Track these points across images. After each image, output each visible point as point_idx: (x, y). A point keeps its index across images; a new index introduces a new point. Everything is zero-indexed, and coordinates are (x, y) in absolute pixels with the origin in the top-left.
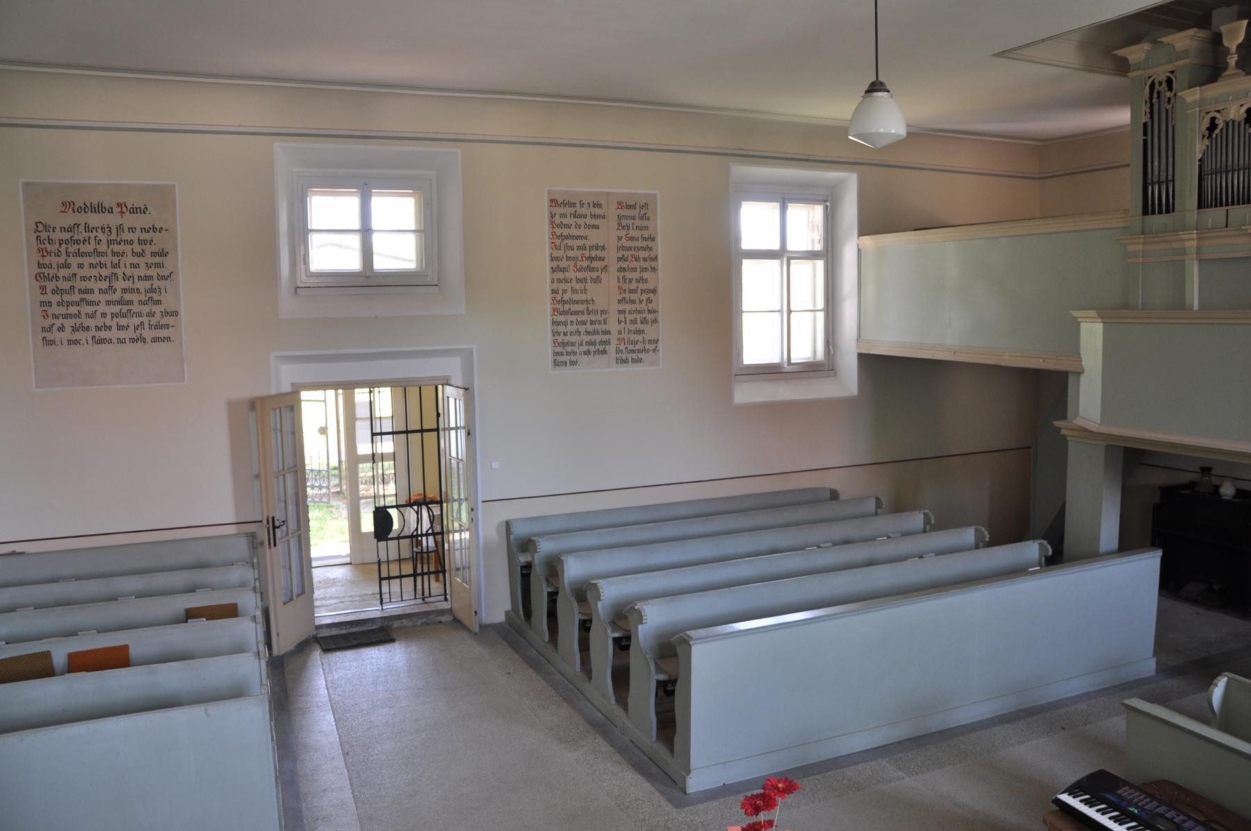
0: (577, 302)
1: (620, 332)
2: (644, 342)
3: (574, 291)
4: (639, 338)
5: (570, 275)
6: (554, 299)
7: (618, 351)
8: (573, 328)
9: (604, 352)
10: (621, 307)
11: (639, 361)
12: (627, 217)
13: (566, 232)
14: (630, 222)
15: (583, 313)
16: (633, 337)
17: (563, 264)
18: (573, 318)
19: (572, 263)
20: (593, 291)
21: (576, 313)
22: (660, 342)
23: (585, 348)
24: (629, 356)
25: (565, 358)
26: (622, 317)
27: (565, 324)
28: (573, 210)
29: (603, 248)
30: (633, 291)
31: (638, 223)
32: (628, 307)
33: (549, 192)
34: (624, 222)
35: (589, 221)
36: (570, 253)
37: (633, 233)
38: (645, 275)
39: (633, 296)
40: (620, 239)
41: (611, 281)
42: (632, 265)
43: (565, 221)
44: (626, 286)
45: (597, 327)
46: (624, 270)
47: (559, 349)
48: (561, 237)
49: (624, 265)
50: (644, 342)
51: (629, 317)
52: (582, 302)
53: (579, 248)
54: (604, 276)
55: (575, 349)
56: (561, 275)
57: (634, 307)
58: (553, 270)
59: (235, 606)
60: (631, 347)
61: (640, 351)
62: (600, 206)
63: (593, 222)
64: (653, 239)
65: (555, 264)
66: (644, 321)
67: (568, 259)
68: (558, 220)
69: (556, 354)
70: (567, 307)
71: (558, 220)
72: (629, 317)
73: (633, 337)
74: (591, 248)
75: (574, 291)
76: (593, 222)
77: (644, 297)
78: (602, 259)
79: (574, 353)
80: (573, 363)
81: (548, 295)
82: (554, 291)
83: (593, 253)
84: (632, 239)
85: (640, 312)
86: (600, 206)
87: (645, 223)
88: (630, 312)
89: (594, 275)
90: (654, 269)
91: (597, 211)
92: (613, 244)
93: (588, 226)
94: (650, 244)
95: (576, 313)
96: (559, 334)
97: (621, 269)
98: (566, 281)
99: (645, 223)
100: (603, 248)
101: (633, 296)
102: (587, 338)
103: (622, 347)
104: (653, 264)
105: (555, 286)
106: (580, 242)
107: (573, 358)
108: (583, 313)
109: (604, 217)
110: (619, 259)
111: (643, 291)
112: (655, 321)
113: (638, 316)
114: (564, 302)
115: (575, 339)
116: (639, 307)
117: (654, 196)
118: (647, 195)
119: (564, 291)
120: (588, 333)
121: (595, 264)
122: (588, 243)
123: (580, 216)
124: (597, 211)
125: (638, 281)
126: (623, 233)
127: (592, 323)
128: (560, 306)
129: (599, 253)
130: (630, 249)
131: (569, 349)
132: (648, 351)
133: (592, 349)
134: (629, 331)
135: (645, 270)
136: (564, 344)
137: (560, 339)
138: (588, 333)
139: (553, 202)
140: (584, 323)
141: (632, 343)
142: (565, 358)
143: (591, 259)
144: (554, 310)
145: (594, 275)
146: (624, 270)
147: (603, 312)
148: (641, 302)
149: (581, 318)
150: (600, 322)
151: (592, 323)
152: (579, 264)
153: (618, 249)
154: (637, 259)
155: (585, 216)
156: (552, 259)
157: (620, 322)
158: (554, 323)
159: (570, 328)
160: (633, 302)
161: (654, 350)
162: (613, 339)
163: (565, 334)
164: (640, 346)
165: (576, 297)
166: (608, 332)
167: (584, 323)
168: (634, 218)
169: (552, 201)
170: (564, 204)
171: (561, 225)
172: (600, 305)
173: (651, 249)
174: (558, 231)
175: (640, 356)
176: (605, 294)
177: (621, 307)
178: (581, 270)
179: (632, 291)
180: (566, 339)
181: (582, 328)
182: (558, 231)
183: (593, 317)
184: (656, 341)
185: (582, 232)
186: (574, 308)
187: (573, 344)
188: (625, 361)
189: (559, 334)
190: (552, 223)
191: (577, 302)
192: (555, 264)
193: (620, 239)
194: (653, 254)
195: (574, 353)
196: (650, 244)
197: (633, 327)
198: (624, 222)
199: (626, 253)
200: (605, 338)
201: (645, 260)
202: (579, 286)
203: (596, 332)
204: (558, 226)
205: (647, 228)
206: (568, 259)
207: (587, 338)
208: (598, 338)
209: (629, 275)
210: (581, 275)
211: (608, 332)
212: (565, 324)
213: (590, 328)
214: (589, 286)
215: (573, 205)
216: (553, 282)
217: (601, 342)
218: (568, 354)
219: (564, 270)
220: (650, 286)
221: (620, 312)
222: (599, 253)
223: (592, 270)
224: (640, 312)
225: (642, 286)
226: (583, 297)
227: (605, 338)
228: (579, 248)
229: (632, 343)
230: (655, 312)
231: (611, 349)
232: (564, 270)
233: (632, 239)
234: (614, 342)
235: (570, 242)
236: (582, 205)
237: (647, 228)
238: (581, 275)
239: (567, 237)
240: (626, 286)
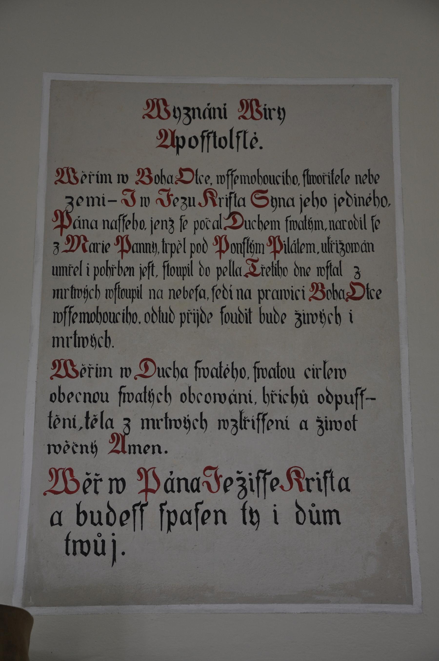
169: (60, 172)
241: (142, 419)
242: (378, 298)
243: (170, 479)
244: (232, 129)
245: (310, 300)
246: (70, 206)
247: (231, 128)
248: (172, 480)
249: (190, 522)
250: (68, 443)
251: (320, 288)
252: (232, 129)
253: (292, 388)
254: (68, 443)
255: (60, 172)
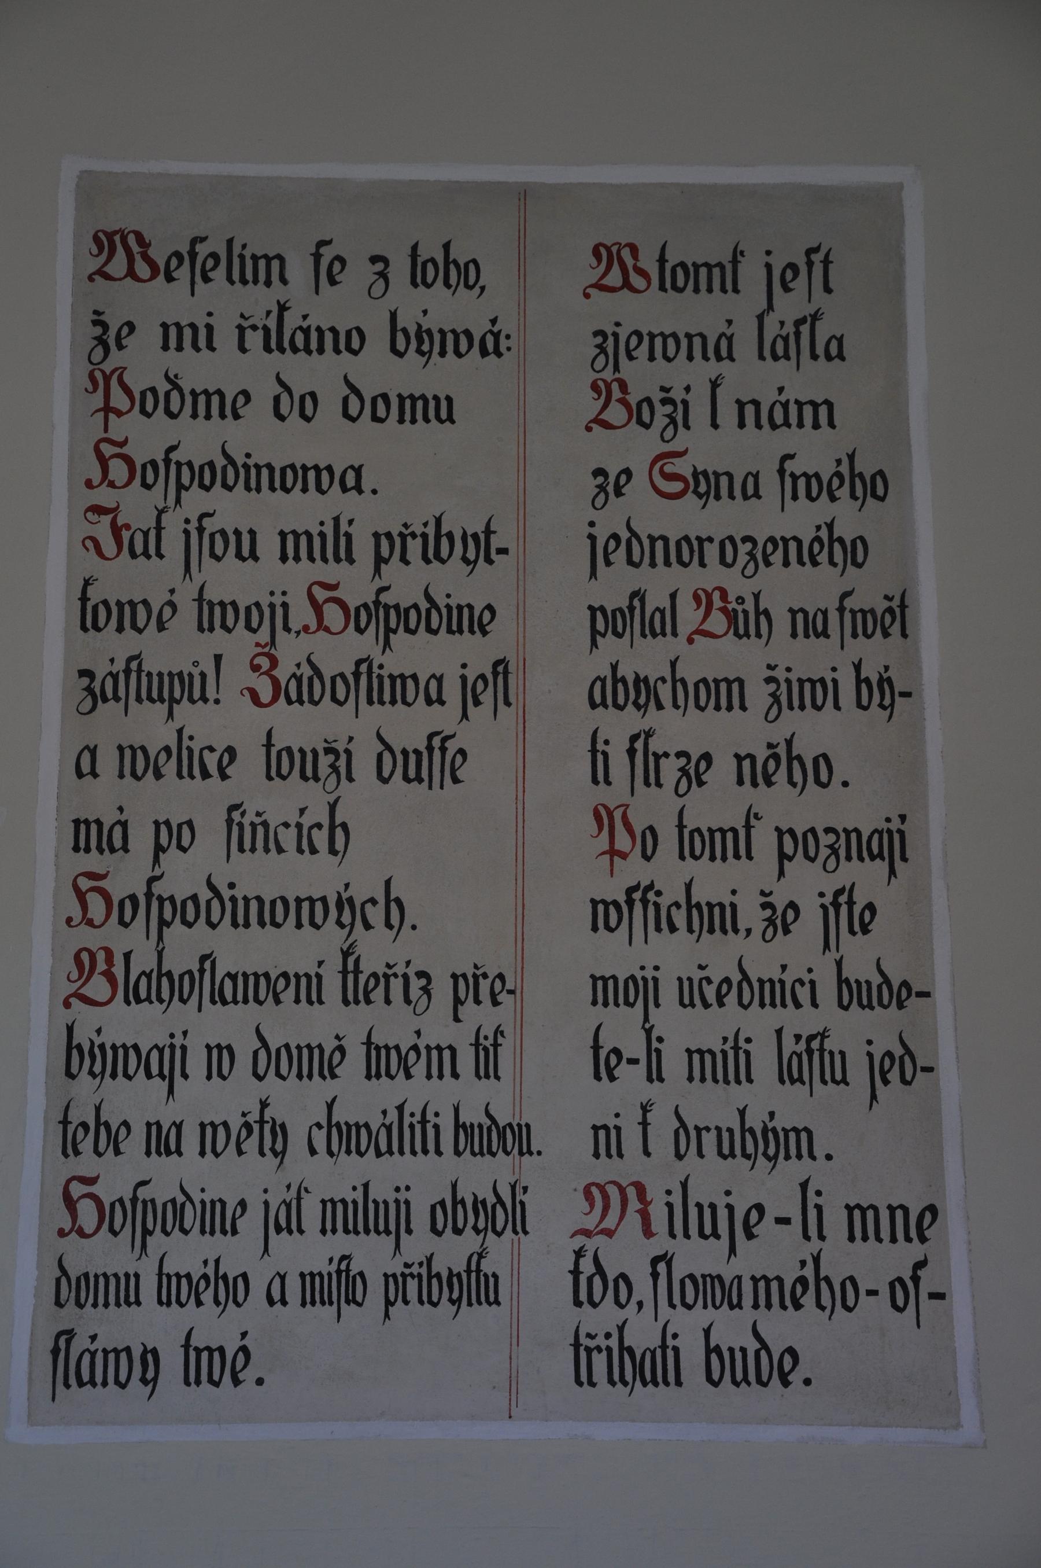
0: (268, 913)
1: (606, 1139)
2: (811, 1221)
3: (246, 833)
4: (775, 1186)
5: (226, 721)
6: (85, 888)
7: (592, 1282)
8: (232, 1099)
9: (475, 1286)
10: (618, 955)
11: (781, 1368)
12: (662, 345)
13: (199, 440)
14: (690, 375)
15: (309, 988)
16: (711, 1178)
17: (169, 651)
18: (232, 1024)
19: (238, 646)
20: (388, 831)
21: (256, 987)
22: (954, 1229)
23: (311, 1251)
24: (688, 1326)
25: (154, 1325)
26: (623, 1029)
27: (167, 1064)
28: (258, 301)
29: (482, 547)
30: (728, 843)
31: (751, 377)
32: (673, 955)
33: (90, 188)
34: (643, 377)
35: (379, 370)
36: (229, 580)
37: (705, 448)
38: (813, 731)
39: (713, 882)
40: (610, 484)
41: (535, 763)
42: (702, 661)
43: (197, 370)
44: (654, 808)
45: (417, 1091)
46: (643, 692)
47: (107, 1254)
48: (169, 470)
49: (645, 658)
50: (811, 1221)
51: (682, 1029)
52: (306, 911)
53: (294, 545)
54: (482, 734)
55: (238, 1253)
56: (151, 726)
57: (720, 956)
58: (94, 690)
59: (745, 426)
60: (698, 1257)
61: (771, 1292)
62: (460, 273)
63: (408, 375)
64: (873, 487)
65: (111, 647)
66: (809, 1062)
67: (213, 615)
68: (144, 363)
69: (73, 1288)
70: (183, 946)
71: (144, 363)
72: (682, 1029)
73: (711, 1178)
74: (390, 546)
75: (246, 833)
76: (408, 375)
77: (807, 884)
78: (474, 621)
79: (230, 1288)
80: (213, 1366)
81: (47, 859)
82: (88, 834)
83: (406, 583)
84: (707, 485)
85: (775, 993)
86: (460, 273)
87: (805, 381)
88: (691, 993)
89: (409, 726)
90: (882, 692)
91: (444, 308)
92: (563, 513)
93: (361, 405)
94: (849, 518)
95: (256, 987)
96: (110, 1137)
97: (612, 691)
98: (190, 761)
99: (805, 381)
100: (482, 547)
101: (713, 882)
102: (337, 1177)
103: (628, 1253)
104: (875, 654)
105: (102, 797)
106: (306, 511)
107: (214, 1325)
108: (309, 988)
109: (492, 345)
110: (605, 623)
111: (795, 844)
112: (900, 1066)
113: (759, 1024)
114: (164, 911)
115: (241, 1177)
116: (764, 959)
117: (886, 202)
118: (822, 196)
119: (174, 836)
120: (345, 1137)
121: (413, 654)
122: (366, 516)
123: (313, 341)
124: (444, 308)
125: (752, 771)
126: (635, 448)
127: (381, 1061)
128: (135, 941)
129: (453, 582)
130: (689, 550)
131: (187, 1253)
132: (846, 1294)
133: (373, 1256)
134: (687, 1136)
135: (815, 693)
136: (142, 1216)
137: (116, 1176)
138: (345, 1137)
139: (117, 250)
140: (319, 1062)
141: (704, 1221)
142: (154, 1325)
143: (384, 617)
144: (84, 964)
145: (409, 726)
146: (643, 692)
147: (471, 986)
148: (780, 920)
149: (290, 1024)
150: (442, 1061)
151: (381, 1061)
152: (291, 652)
153: (598, 556)
154: (746, 621)
155: (351, 341)
156: (90, 615)
157: (605, 1064)
158: (76, 1055)
159: (200, 1099)
160: (719, 919)
161: (904, 1292)
162: (555, 1190)
163: (162, 1141)
164: (775, 1252)
165: (260, 876)
166: (516, 1138)
167: (319, 1062)
168: (723, 350)
169: (106, 242)
170: (195, 262)
171: (167, 399)
172: (447, 936)
173: (855, 553)
174: (146, 437)
175: (781, 1328)
176: (492, 860)
177: (618, 955)
178: (306, 688)
179: (697, 843)
180: (166, 1178)
181: (298, 1103)
182: (146, 437)
183: (394, 1024)
184: (921, 1222)
185: (325, 441)
186: (239, 950)
187: (219, 1219)
188: (651, 1369)
189: (110, 1137)
190: (101, 381)
191: (268, 913)
192: (111, 647)
193: (610, 484)
194: (869, 590)
195: (230, 1288)
196: (849, 518)
197: (713, 1106)
198: (643, 377)
199: (659, 584)
200: (480, 1176)
201: (809, 625)
202: (283, 802)
203: (407, 1133)
204: (145, 403)
205: (822, 413)
206: (213, 615)
207: (337, 1177)
208: (422, 1178)
209: (676, 729)
210: (300, 726)
211: (516, 1138)
212: (167, 1064)
213: (362, 1099)
214: (363, 799)
215: (263, 268)
216: (85, 765)
217: (450, 1213)
218: (175, 1288)
219: (178, 689)
220: (860, 810)
221: (605, 990)
222: (453, 582)
223: (397, 689)
224: (775, 993)
225: (783, 805)
226: (315, 876)
227: (480, 1176)
228: (294, 545)
229: (704, 1221)
230: (902, 994)
231: (536, 1264)
232: (178, 689)
233: (707, 485)
234: (556, 1214)
235: (230, 508)
236: (328, 269)
237: (822, 413)
238: (300, 726)
239: (206, 476)
240: (654, 808)
241: (733, 360)
242: (224, 776)
243: (781, 336)
244: (676, 591)
245: (690, 641)
246: (381, 282)
247: (387, 878)
248: (93, 1354)
249: (787, 357)
250: (342, 1042)
251: (101, 966)
252: (676, 591)
253: (388, 883)
254: (342, 1042)
255: (106, 242)
